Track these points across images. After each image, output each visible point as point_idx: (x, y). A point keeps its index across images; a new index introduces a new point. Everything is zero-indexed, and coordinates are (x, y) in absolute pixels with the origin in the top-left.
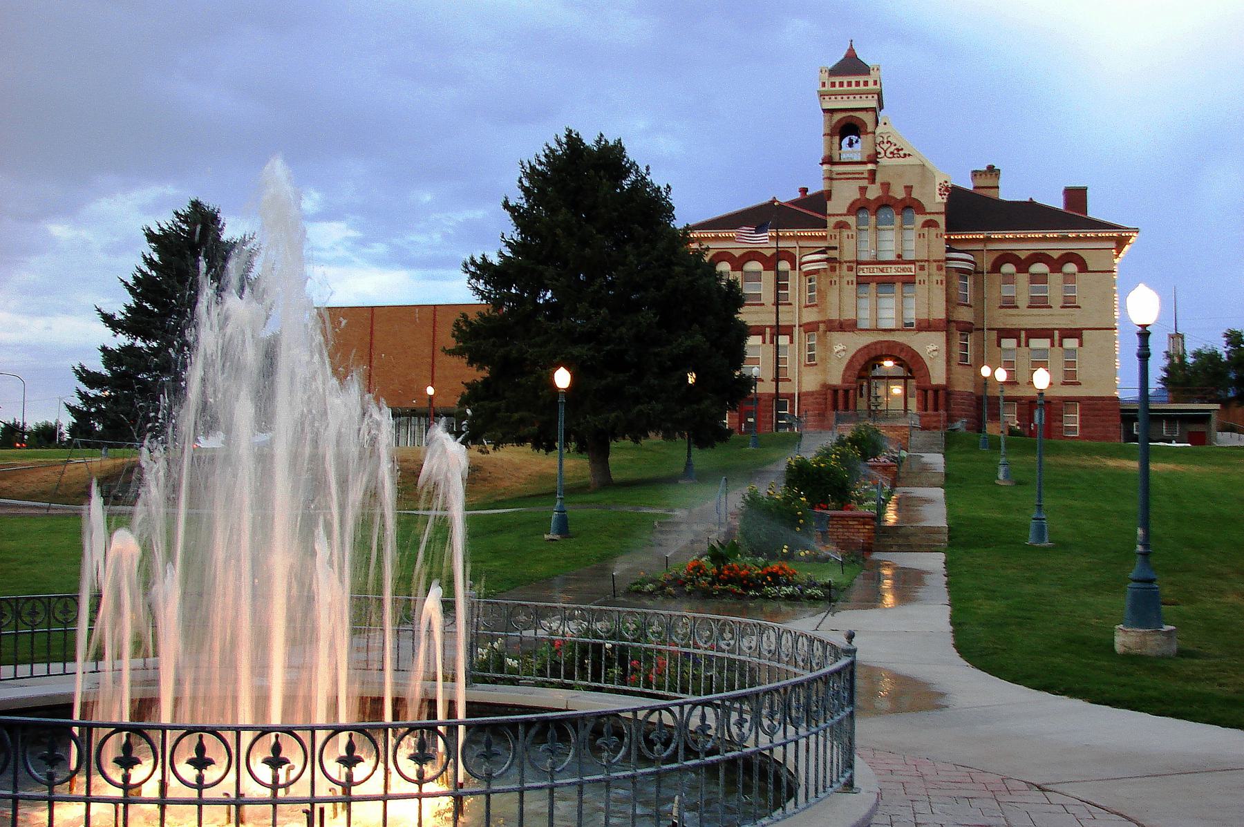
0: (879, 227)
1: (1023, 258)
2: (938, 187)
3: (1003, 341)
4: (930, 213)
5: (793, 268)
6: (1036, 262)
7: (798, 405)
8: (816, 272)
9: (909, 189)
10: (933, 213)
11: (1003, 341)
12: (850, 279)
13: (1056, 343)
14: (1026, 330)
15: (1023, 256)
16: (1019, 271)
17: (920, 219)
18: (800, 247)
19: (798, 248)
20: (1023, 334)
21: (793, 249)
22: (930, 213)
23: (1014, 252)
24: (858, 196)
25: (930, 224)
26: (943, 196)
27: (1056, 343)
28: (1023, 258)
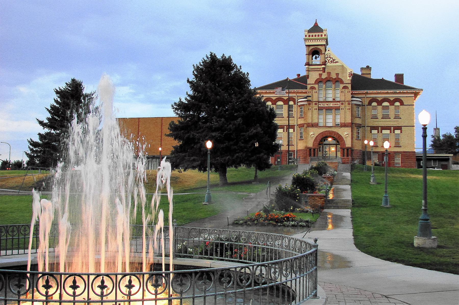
2: (348, 74)
3: (383, 131)
4: (345, 84)
5: (295, 104)
8: (303, 105)
9: (337, 74)
10: (346, 84)
15: (380, 99)
17: (342, 86)
20: (380, 128)
22: (345, 84)
25: (345, 88)
26: (350, 77)
28: (380, 100)
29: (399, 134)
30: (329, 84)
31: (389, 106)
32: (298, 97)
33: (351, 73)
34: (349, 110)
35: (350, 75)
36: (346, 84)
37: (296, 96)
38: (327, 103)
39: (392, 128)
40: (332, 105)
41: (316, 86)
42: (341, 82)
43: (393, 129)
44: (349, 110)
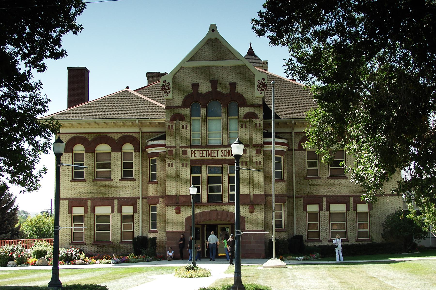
0: (229, 117)
1: (90, 139)
2: (257, 84)
3: (123, 208)
4: (251, 106)
5: (137, 149)
6: (124, 144)
7: (368, 262)
8: (157, 154)
9: (233, 85)
10: (254, 106)
11: (123, 208)
12: (185, 162)
13: (324, 207)
14: (118, 199)
15: (90, 138)
16: (87, 151)
17: (243, 111)
18: (142, 132)
19: (140, 133)
20: (89, 203)
21: (137, 134)
22: (251, 106)
23: (83, 135)
24: (191, 91)
25: (251, 116)
26: (261, 92)
27: (324, 207)
28: (90, 139)
29: (366, 213)
30: (215, 106)
31: (111, 153)
32: (144, 134)
33: (263, 82)
34: (171, 163)
35: (261, 85)
36: (254, 106)
37: (139, 132)
38: (209, 149)
39: (324, 199)
40: (220, 154)
41: (186, 112)
42: (242, 102)
43: (118, 204)
44: (171, 163)
